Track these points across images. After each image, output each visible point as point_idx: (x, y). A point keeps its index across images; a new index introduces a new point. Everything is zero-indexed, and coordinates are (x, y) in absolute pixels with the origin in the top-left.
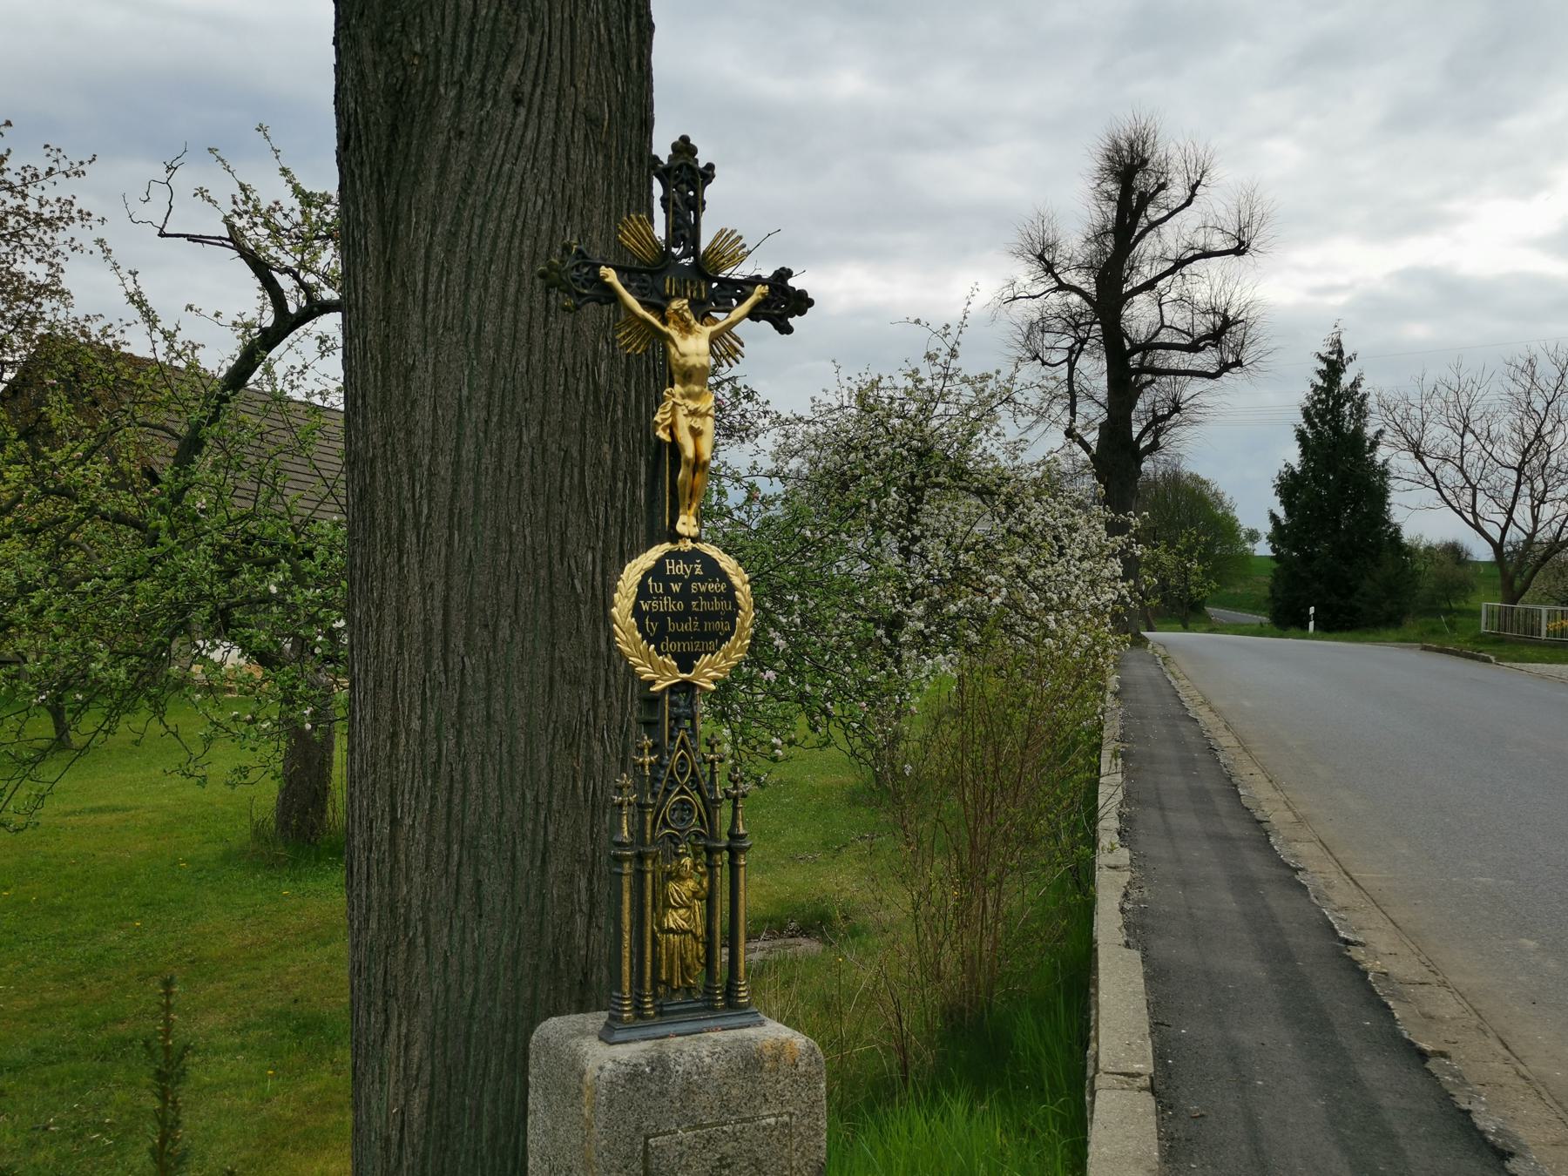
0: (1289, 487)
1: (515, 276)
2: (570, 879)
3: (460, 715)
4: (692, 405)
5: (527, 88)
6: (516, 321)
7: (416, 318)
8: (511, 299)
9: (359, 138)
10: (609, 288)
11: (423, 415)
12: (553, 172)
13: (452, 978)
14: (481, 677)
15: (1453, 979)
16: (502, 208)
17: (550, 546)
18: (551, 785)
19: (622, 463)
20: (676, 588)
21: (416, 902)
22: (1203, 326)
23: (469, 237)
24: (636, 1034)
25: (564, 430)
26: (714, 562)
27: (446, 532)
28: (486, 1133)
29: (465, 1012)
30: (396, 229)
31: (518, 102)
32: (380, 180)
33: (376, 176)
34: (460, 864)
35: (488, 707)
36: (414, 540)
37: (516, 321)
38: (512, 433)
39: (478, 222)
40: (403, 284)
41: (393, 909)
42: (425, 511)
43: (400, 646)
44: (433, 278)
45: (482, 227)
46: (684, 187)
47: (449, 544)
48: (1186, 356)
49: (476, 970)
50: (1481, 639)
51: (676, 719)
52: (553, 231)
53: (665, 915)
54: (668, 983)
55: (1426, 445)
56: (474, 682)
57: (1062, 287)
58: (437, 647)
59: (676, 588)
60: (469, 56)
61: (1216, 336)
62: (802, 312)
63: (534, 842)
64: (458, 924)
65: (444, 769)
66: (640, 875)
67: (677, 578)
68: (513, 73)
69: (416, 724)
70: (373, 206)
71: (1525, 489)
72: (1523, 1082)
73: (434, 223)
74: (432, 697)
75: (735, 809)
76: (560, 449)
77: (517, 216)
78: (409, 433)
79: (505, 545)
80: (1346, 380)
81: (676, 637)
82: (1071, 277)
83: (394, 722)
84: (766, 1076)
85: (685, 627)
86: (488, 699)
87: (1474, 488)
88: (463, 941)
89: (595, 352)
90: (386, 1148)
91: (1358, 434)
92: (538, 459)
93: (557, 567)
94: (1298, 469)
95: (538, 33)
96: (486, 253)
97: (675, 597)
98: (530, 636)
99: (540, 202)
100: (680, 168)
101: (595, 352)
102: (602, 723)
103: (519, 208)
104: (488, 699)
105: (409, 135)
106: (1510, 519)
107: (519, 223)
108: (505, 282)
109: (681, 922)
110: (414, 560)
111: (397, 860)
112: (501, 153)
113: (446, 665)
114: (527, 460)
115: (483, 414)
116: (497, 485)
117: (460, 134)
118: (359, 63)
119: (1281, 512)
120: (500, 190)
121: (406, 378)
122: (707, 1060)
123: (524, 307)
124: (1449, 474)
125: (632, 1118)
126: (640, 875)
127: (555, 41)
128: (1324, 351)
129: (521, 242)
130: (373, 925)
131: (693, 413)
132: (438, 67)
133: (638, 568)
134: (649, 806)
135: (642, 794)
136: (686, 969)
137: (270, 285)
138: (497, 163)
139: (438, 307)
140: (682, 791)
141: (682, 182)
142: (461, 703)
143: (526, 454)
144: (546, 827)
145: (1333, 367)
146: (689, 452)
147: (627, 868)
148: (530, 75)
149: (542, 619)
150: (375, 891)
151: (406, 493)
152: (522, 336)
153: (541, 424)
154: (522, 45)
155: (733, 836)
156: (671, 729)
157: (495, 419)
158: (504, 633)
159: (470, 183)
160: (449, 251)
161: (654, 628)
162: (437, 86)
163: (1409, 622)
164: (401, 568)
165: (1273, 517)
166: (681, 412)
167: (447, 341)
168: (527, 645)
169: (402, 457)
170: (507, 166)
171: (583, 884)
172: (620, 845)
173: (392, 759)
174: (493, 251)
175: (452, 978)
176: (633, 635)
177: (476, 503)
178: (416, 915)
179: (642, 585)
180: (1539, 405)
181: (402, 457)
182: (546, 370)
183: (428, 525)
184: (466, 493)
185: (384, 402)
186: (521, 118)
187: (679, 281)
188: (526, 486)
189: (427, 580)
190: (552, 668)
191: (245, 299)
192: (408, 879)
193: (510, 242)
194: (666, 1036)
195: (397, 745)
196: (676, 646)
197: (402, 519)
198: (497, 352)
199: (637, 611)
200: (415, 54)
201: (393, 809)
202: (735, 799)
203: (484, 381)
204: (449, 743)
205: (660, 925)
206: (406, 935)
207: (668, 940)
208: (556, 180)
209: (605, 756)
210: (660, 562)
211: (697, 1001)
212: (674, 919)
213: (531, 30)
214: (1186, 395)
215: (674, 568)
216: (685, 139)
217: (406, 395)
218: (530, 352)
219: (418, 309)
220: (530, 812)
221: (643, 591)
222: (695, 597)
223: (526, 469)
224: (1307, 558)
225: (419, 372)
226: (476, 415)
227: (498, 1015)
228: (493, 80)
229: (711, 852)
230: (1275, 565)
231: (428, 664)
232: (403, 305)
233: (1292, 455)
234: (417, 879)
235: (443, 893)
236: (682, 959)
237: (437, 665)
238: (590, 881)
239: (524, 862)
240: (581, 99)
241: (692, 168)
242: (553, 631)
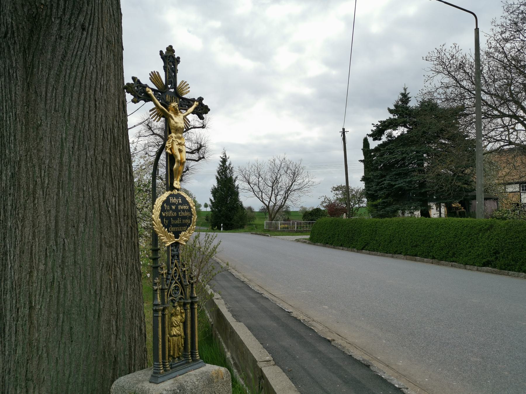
0: (215, 192)
1: (83, 94)
2: (109, 322)
3: (63, 262)
4: (179, 141)
5: (87, 25)
6: (84, 110)
7: (42, 105)
8: (82, 102)
9: (13, 33)
11: (46, 144)
12: (96, 57)
14: (72, 246)
15: (315, 319)
16: (78, 68)
17: (99, 196)
18: (101, 286)
19: (123, 166)
22: (195, 147)
23: (65, 77)
24: (166, 378)
25: (103, 152)
26: (185, 198)
27: (56, 190)
29: (66, 381)
30: (32, 70)
31: (83, 29)
32: (25, 51)
33: (23, 49)
34: (63, 322)
35: (75, 258)
36: (41, 193)
37: (84, 110)
38: (83, 152)
39: (68, 71)
40: (36, 92)
42: (47, 182)
45: (70, 74)
46: (171, 63)
48: (190, 155)
49: (70, 363)
50: (265, 231)
52: (97, 79)
53: (171, 330)
55: (251, 181)
56: (69, 248)
57: (154, 134)
58: (52, 236)
59: (174, 207)
60: (64, 9)
61: (198, 150)
62: (206, 113)
63: (95, 309)
64: (62, 346)
65: (56, 284)
66: (163, 315)
67: (174, 204)
68: (81, 18)
69: (42, 267)
71: (273, 193)
72: (349, 345)
73: (50, 70)
74: (50, 256)
75: (192, 287)
76: (102, 159)
77: (83, 71)
79: (81, 195)
80: (227, 164)
82: (156, 131)
83: (31, 267)
84: (215, 385)
86: (75, 255)
87: (262, 192)
88: (64, 352)
89: (113, 125)
91: (231, 177)
92: (93, 163)
93: (102, 203)
94: (216, 187)
95: (90, 5)
96: (72, 84)
97: (174, 211)
98: (92, 230)
99: (92, 67)
100: (169, 57)
101: (113, 125)
102: (120, 261)
103: (84, 69)
105: (39, 35)
106: (270, 200)
107: (84, 74)
108: (79, 94)
109: (178, 332)
110: (41, 202)
111: (31, 323)
112: (77, 47)
113: (56, 242)
114: (90, 163)
115: (72, 145)
116: (78, 172)
117: (61, 37)
118: (14, 4)
119: (212, 199)
120: (77, 61)
121: (37, 129)
122: (196, 383)
123: (87, 105)
124: (256, 188)
126: (163, 315)
127: (96, 10)
128: (222, 156)
129: (85, 81)
130: (19, 351)
131: (179, 144)
132: (51, 11)
133: (161, 200)
134: (166, 289)
135: (163, 284)
138: (76, 51)
139: (52, 102)
140: (176, 283)
141: (170, 62)
142: (63, 257)
143: (89, 161)
144: (99, 303)
145: (224, 161)
147: (160, 313)
148: (88, 20)
149: (97, 223)
151: (37, 173)
152: (87, 116)
153: (94, 150)
154: (85, 9)
155: (192, 298)
156: (172, 260)
157: (76, 147)
158: (81, 229)
159: (65, 57)
160: (57, 81)
162: (51, 18)
163: (246, 227)
164: (34, 205)
165: (211, 200)
166: (175, 143)
167: (56, 115)
168: (91, 233)
169: (35, 161)
170: (79, 53)
171: (114, 323)
172: (157, 305)
173: (29, 283)
174: (74, 83)
176: (160, 225)
177: (69, 178)
179: (162, 206)
180: (277, 171)
181: (35, 161)
182: (96, 130)
183: (48, 187)
184: (65, 175)
185: (26, 138)
186: (84, 36)
187: (170, 97)
188: (89, 173)
189: (47, 209)
190: (101, 242)
192: (38, 331)
193: (81, 81)
194: (176, 376)
195: (32, 276)
196: (173, 229)
198: (77, 122)
199: (161, 216)
200: (42, 4)
201: (30, 302)
202: (192, 284)
203: (72, 132)
205: (170, 334)
206: (38, 354)
207: (173, 339)
208: (97, 60)
209: (121, 274)
210: (168, 198)
211: (183, 361)
213: (88, 5)
214: (190, 166)
215: (173, 200)
216: (171, 47)
218: (89, 123)
219: (43, 102)
220: (93, 298)
221: (163, 209)
222: (180, 211)
223: (89, 166)
224: (220, 211)
225: (44, 127)
226: (68, 145)
227: (80, 380)
228: (74, 19)
230: (211, 213)
231: (48, 242)
234: (43, 330)
235: (55, 334)
236: (178, 346)
237: (52, 243)
238: (116, 322)
240: (105, 33)
241: (173, 57)
242: (101, 228)
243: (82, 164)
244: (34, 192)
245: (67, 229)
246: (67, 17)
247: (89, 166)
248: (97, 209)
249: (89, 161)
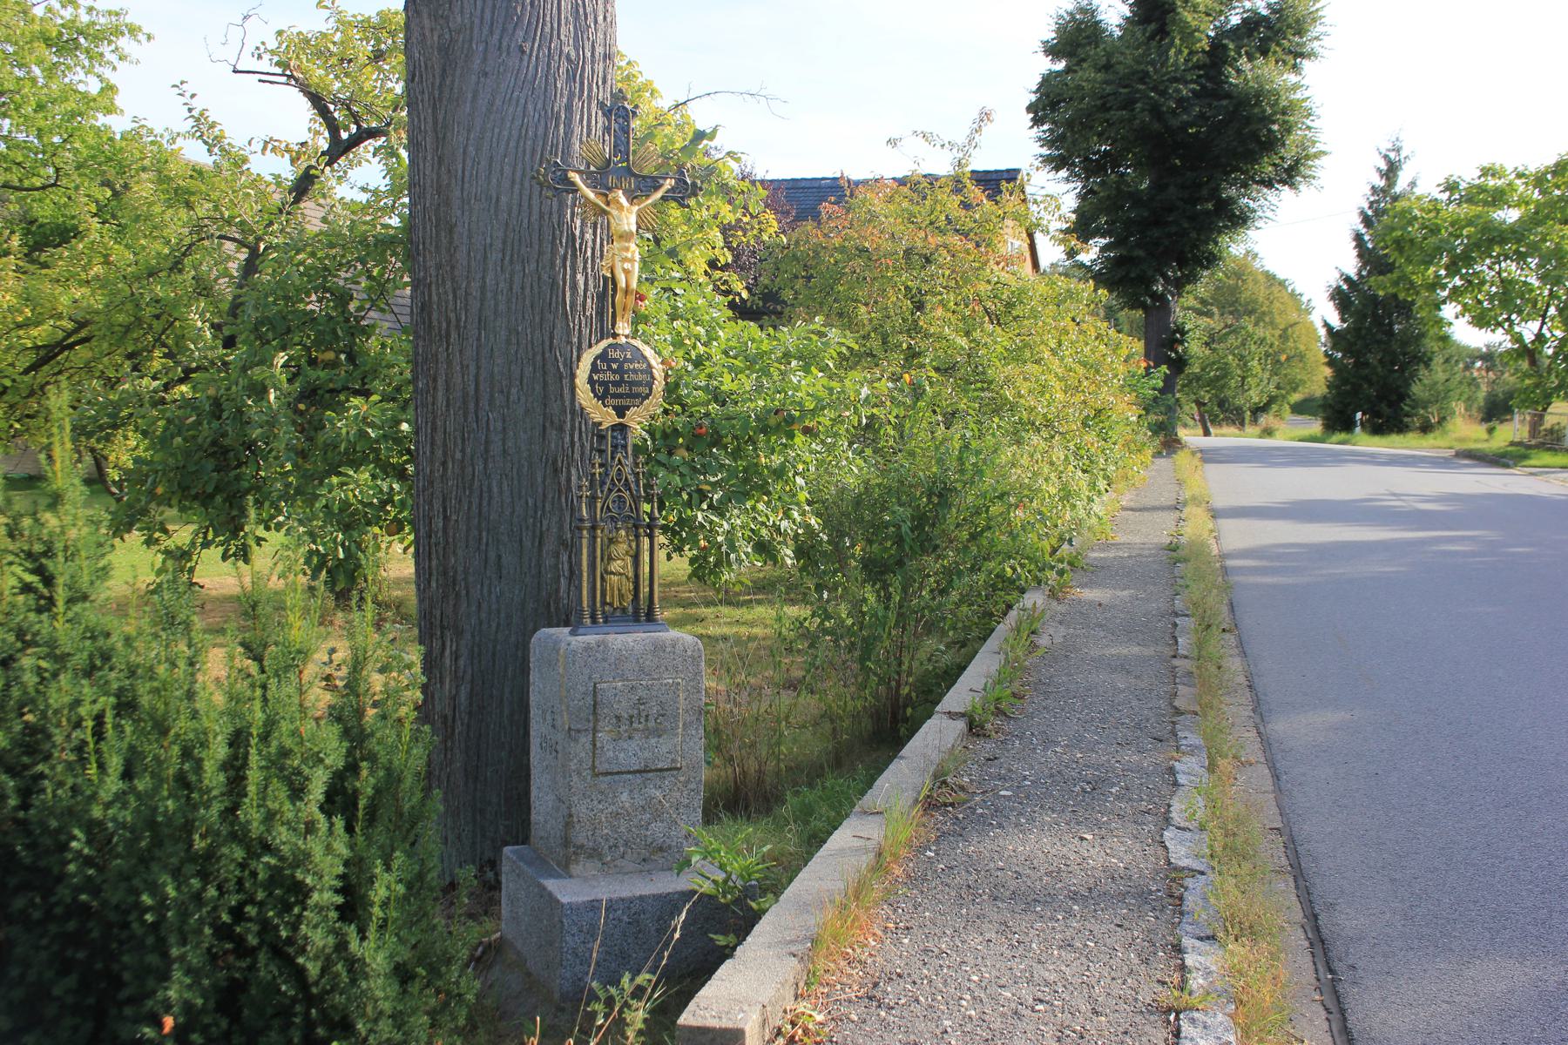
2: (557, 555)
7: (457, 193)
10: (573, 184)
13: (483, 615)
14: (499, 425)
20: (615, 366)
21: (460, 569)
28: (506, 712)
38: (518, 267)
41: (445, 573)
43: (448, 405)
44: (468, 168)
47: (479, 339)
49: (499, 611)
51: (615, 447)
54: (611, 604)
58: (472, 406)
59: (615, 366)
67: (615, 361)
69: (458, 455)
70: (430, 120)
73: (469, 131)
78: (453, 268)
79: (514, 340)
80: (1401, 185)
81: (615, 396)
85: (620, 390)
86: (504, 440)
88: (490, 592)
90: (445, 722)
97: (614, 372)
104: (504, 440)
116: (509, 301)
117: (486, 74)
125: (586, 671)
130: (434, 584)
136: (621, 596)
137: (324, 112)
142: (487, 442)
143: (528, 281)
146: (622, 284)
149: (538, 388)
150: (434, 563)
151: (451, 306)
161: (602, 392)
169: (449, 284)
171: (565, 558)
175: (483, 615)
178: (460, 577)
179: (594, 364)
181: (449, 284)
191: (293, 119)
196: (615, 402)
197: (449, 323)
199: (591, 381)
204: (480, 467)
210: (605, 351)
212: (615, 566)
215: (612, 354)
217: (451, 243)
220: (531, 512)
221: (594, 368)
222: (626, 372)
223: (528, 290)
226: (494, 256)
227: (513, 639)
229: (636, 527)
232: (449, 185)
233: (1351, 264)
234: (460, 552)
237: (471, 417)
239: (527, 544)
243: (516, 288)
244: (448, 335)
245: (492, 396)
246: (496, 37)
247: (528, 290)
248: (539, 363)
249: (528, 281)
